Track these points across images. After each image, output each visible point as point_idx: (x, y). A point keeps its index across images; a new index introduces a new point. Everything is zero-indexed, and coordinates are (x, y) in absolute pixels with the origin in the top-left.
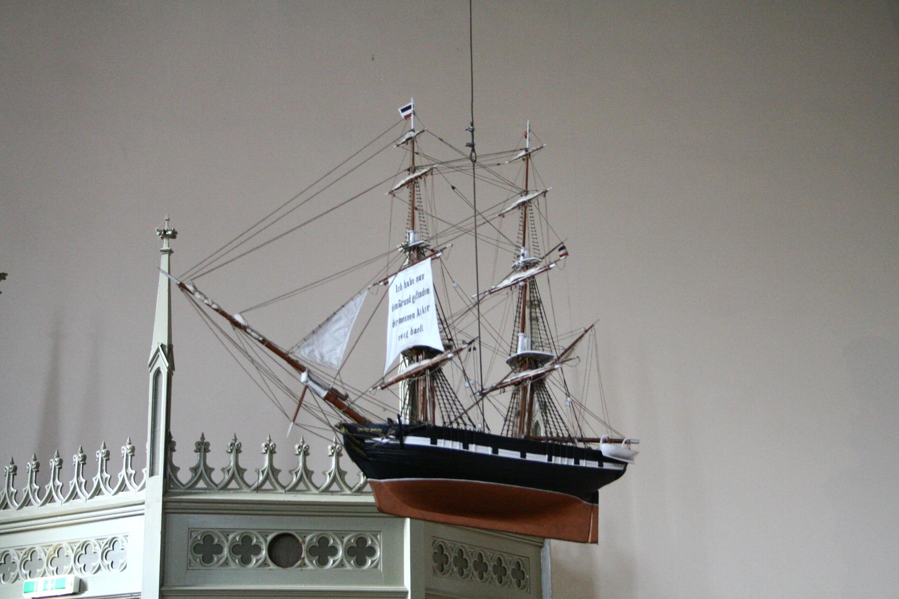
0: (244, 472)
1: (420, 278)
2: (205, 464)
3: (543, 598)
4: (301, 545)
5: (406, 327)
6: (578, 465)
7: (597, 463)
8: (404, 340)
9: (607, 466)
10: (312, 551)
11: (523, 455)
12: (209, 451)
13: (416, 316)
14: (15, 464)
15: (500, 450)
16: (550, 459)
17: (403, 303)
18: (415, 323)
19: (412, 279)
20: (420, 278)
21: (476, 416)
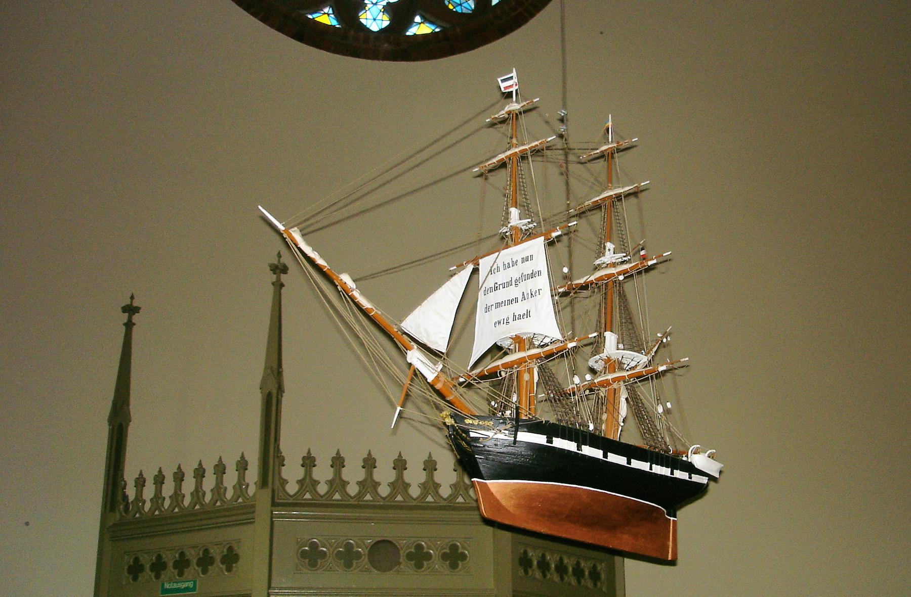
0: (360, 482)
1: (527, 259)
2: (311, 478)
3: (619, 593)
4: (399, 551)
5: (506, 312)
6: (673, 476)
7: (601, 452)
8: (503, 327)
9: (696, 478)
10: (410, 556)
11: (550, 441)
12: (125, 324)
13: (520, 300)
14: (587, 161)
15: (632, 460)
16: (672, 473)
17: (501, 286)
18: (519, 308)
19: (514, 260)
20: (527, 259)
21: (410, 390)
